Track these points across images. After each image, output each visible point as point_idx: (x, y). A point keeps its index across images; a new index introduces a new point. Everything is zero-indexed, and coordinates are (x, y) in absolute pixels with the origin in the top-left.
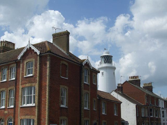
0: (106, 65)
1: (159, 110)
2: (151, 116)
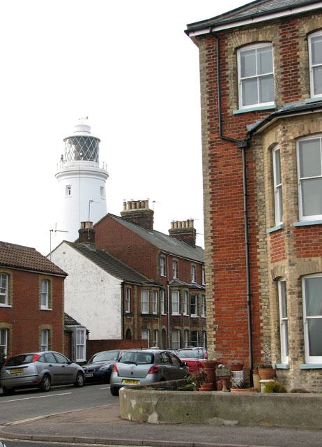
0: (84, 164)
1: (200, 296)
2: (192, 316)
